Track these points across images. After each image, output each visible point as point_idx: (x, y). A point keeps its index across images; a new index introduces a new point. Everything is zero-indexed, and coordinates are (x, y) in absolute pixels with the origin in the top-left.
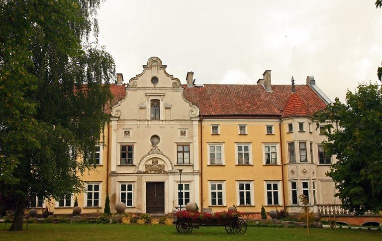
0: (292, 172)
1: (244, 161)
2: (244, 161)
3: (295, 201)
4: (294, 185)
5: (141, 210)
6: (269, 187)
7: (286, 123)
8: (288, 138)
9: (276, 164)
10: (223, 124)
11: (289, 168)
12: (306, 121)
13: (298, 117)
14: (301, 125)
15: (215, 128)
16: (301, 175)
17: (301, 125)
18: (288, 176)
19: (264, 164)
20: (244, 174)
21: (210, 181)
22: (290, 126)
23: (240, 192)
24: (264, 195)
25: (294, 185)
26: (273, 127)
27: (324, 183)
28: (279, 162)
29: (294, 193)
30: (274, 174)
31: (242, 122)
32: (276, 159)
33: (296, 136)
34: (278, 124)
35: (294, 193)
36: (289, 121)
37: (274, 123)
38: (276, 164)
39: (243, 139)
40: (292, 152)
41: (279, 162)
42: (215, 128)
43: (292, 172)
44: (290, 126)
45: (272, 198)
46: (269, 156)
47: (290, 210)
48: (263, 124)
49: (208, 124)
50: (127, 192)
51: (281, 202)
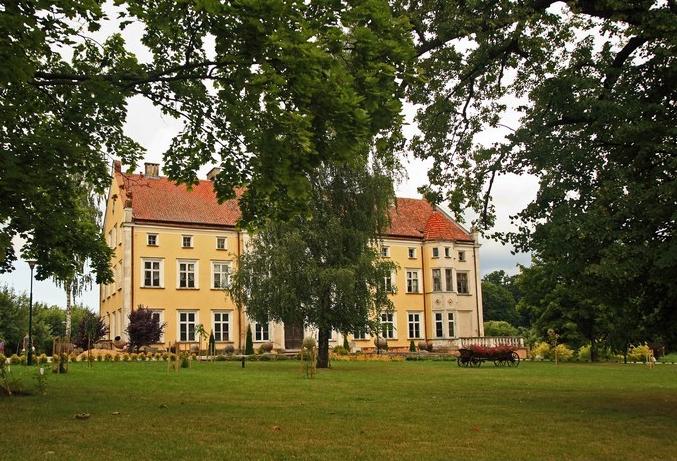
0: (437, 302)
1: (187, 283)
2: (187, 283)
3: (439, 333)
4: (439, 317)
5: (280, 345)
6: (183, 317)
7: (430, 247)
8: (432, 264)
9: (417, 293)
10: (197, 237)
11: (433, 298)
12: (450, 245)
13: (444, 241)
14: (447, 250)
15: (152, 239)
16: (447, 306)
17: (447, 250)
18: (433, 307)
19: (178, 286)
20: (187, 300)
21: (409, 311)
22: (436, 251)
23: (182, 325)
24: (176, 329)
25: (439, 317)
26: (192, 238)
27: (462, 314)
28: (421, 290)
29: (439, 326)
30: (416, 303)
31: (187, 232)
32: (417, 287)
33: (442, 263)
34: (419, 247)
35: (439, 326)
36: (435, 245)
37: (416, 245)
38: (417, 293)
39: (187, 254)
40: (437, 280)
41: (421, 290)
42: (152, 239)
43: (437, 302)
44: (436, 251)
45: (414, 330)
46: (410, 283)
47: (436, 344)
48: (212, 236)
49: (143, 233)
50: (222, 322)
51: (422, 335)
